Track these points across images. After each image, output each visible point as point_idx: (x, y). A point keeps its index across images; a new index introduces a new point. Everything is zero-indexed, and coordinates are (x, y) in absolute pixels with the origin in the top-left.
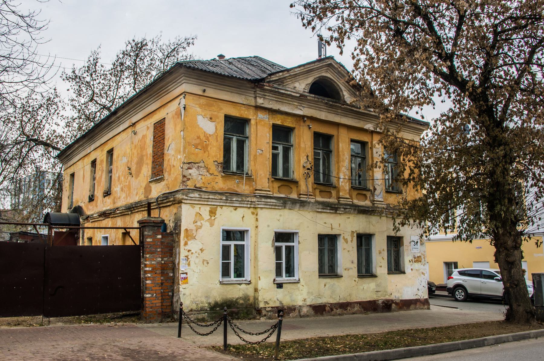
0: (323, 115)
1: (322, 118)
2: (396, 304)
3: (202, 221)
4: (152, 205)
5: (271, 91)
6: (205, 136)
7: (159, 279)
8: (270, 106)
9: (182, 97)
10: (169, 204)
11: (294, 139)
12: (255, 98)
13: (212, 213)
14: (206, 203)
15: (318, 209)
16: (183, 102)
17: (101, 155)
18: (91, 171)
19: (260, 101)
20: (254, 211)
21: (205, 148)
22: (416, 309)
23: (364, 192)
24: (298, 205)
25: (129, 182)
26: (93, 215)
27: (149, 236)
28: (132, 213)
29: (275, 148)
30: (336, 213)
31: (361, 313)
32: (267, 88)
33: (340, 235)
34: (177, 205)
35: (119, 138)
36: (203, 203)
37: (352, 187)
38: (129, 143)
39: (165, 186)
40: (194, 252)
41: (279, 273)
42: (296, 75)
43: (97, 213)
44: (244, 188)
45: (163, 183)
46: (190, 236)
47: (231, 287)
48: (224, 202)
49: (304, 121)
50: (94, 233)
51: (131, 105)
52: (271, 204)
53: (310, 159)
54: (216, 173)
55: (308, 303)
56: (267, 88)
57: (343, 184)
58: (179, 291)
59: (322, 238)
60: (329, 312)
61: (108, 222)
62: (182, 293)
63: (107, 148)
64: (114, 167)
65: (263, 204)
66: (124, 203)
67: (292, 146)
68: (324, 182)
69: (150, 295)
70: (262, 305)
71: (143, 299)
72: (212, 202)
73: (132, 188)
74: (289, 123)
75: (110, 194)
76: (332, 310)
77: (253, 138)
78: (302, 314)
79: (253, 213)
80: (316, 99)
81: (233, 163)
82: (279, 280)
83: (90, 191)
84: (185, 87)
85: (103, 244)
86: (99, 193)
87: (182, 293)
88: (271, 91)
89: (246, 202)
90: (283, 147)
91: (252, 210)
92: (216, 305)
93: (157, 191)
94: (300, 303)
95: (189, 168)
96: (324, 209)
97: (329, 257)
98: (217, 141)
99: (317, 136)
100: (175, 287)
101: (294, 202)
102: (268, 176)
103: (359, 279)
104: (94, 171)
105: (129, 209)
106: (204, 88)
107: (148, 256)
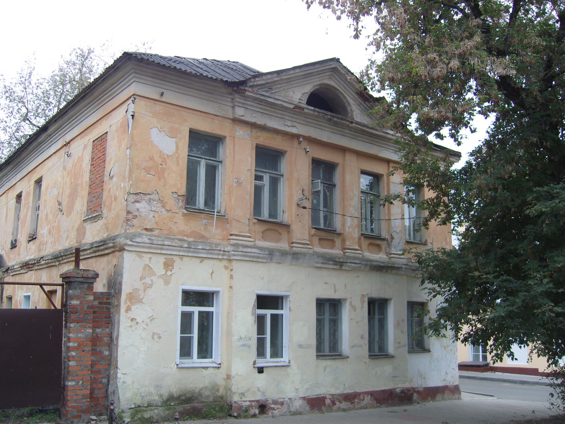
0: (325, 136)
1: (323, 140)
2: (418, 392)
3: (153, 278)
4: (81, 253)
5: (255, 99)
6: (160, 157)
7: (88, 359)
8: (253, 120)
9: (130, 101)
10: (107, 252)
11: (284, 166)
12: (233, 107)
13: (168, 265)
14: (159, 251)
15: (317, 263)
16: (132, 108)
17: (27, 187)
18: (16, 208)
19: (240, 112)
20: (227, 264)
21: (161, 175)
22: (443, 399)
23: (378, 242)
24: (289, 257)
25: (59, 221)
26: (13, 266)
27: (77, 298)
28: (60, 264)
29: (258, 178)
30: (340, 269)
31: (372, 407)
32: (250, 94)
33: (345, 300)
34: (117, 254)
35: (49, 163)
36: (155, 251)
37: (362, 234)
38: (61, 169)
39: (104, 227)
40: (140, 322)
41: (261, 353)
42: (289, 80)
43: (20, 263)
44: (214, 232)
45: (100, 223)
46: (133, 298)
47: (192, 372)
48: (185, 251)
49: (300, 143)
50: (14, 291)
51: (66, 118)
52: (252, 254)
53: (306, 193)
54: (175, 209)
55: (302, 395)
56: (250, 94)
57: (350, 230)
58: (116, 377)
59: (321, 303)
60: (329, 406)
61: (30, 276)
62: (121, 381)
63: (35, 177)
64: (42, 202)
65: (241, 256)
66: (52, 251)
67: (282, 175)
68: (326, 231)
69: (73, 383)
70: (236, 398)
71: (64, 388)
72: (167, 250)
73: (61, 232)
74: (276, 143)
75: (36, 238)
76: (334, 403)
77: (228, 162)
78: (293, 409)
79: (226, 268)
80: (316, 113)
81: (200, 198)
82: (261, 363)
83: (13, 234)
84: (134, 88)
85: (23, 306)
86: (22, 238)
87: (121, 381)
88: (255, 99)
89: (216, 252)
90: (270, 177)
91: (225, 263)
92: (171, 398)
93: (94, 234)
94: (292, 395)
95: (136, 201)
96: (324, 264)
97: (330, 330)
98: (178, 165)
99: (316, 163)
100: (112, 372)
101: (284, 254)
102: (248, 216)
103: (371, 360)
104: (18, 210)
105: (56, 258)
106: (162, 90)
107: (72, 325)
